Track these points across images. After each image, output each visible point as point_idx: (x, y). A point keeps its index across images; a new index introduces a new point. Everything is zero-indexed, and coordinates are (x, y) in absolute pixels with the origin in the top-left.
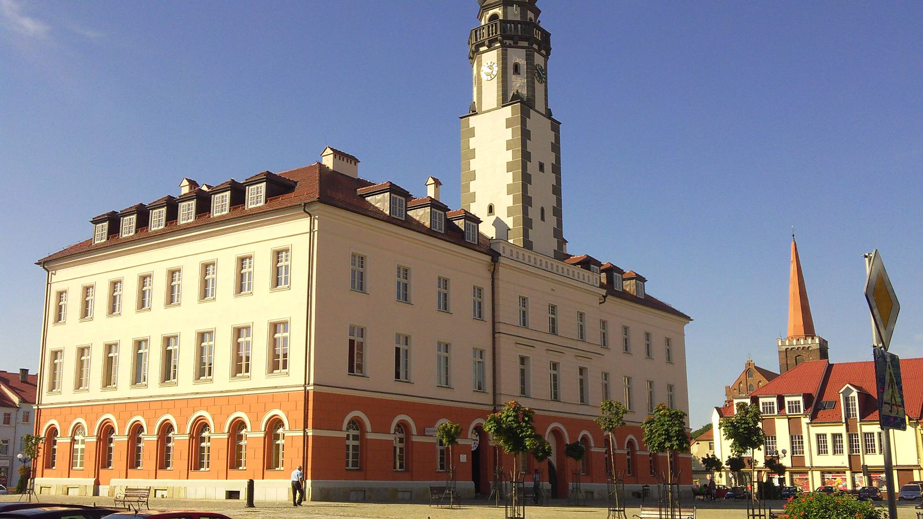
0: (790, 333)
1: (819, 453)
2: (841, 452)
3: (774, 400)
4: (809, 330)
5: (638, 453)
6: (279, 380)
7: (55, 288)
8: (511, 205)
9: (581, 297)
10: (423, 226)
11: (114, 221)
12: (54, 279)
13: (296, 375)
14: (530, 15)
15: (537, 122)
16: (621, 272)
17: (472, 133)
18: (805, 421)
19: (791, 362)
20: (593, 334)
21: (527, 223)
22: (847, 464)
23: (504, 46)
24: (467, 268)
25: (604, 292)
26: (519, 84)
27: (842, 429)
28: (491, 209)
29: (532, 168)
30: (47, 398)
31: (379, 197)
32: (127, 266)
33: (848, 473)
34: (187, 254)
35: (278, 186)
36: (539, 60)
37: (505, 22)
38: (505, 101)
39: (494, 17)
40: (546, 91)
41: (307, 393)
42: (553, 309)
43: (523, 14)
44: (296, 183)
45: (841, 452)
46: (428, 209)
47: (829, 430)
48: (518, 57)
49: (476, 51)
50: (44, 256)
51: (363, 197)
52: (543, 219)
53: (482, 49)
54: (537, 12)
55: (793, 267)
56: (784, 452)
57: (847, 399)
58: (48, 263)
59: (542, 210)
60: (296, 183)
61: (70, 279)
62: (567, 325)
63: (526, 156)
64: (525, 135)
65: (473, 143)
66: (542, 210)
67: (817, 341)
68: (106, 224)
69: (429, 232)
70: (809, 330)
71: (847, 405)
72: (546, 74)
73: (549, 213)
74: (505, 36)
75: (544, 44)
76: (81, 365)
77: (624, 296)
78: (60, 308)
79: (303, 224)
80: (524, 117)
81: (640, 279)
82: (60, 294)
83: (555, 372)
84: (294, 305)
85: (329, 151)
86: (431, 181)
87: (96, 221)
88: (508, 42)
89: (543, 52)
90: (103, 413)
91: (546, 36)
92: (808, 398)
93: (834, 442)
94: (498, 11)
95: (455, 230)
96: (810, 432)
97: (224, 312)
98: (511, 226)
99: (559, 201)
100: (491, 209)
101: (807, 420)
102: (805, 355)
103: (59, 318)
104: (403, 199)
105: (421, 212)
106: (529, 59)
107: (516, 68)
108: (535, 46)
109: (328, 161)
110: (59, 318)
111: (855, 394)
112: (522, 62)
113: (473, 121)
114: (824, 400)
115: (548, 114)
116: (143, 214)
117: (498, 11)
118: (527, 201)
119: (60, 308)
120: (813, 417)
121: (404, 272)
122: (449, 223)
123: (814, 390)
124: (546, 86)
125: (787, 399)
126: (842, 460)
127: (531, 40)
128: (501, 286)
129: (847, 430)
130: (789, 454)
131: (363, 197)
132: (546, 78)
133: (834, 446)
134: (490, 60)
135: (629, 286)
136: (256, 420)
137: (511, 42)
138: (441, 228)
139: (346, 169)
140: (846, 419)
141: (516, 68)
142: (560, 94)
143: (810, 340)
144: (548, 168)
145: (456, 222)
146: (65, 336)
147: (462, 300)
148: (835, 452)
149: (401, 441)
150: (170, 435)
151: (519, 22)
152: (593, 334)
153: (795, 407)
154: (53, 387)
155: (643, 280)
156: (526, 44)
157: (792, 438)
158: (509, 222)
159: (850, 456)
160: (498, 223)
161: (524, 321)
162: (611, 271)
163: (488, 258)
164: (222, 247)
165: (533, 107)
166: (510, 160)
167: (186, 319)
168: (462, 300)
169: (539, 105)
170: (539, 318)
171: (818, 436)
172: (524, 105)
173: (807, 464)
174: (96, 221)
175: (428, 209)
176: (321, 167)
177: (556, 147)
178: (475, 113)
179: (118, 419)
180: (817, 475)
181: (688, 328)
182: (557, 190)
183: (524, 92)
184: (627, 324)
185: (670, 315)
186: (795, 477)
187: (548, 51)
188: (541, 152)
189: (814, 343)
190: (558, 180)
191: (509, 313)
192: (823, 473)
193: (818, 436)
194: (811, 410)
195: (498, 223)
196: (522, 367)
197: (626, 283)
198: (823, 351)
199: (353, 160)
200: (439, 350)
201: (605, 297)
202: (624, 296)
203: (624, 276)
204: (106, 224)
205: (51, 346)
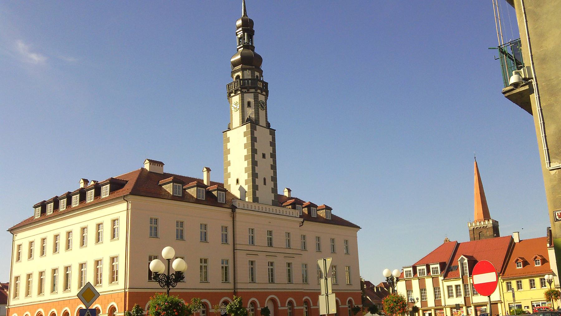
0: (476, 218)
1: (449, 297)
2: (460, 295)
3: (425, 267)
4: (486, 215)
5: (312, 307)
6: (114, 287)
7: (17, 243)
8: (247, 178)
9: (288, 223)
10: (193, 197)
11: (43, 206)
12: (16, 238)
13: (121, 285)
14: (257, 74)
15: (261, 132)
16: (316, 206)
17: (228, 140)
18: (441, 278)
19: (477, 236)
20: (296, 243)
21: (255, 188)
22: (463, 303)
23: (242, 93)
24: (216, 217)
25: (302, 220)
26: (250, 112)
27: (460, 282)
28: (237, 181)
29: (258, 157)
30: (12, 302)
31: (168, 185)
32: (48, 230)
33: (464, 308)
34: (73, 224)
35: (116, 185)
36: (261, 98)
37: (243, 80)
38: (243, 122)
39: (238, 77)
40: (266, 114)
41: (125, 293)
42: (270, 233)
43: (253, 74)
44: (127, 181)
45: (460, 295)
46: (195, 188)
47: (453, 283)
48: (250, 98)
49: (229, 96)
50: (11, 226)
51: (161, 186)
52: (265, 184)
53: (232, 95)
54: (261, 72)
55: (476, 177)
56: (417, 299)
57: (462, 264)
58: (13, 230)
59: (265, 179)
60: (127, 181)
61: (23, 237)
62: (279, 241)
63: (254, 151)
64: (253, 140)
65: (229, 146)
66: (265, 179)
67: (491, 222)
68: (40, 208)
69: (197, 201)
70: (486, 215)
71: (463, 268)
72: (266, 105)
73: (269, 181)
74: (242, 87)
75: (265, 88)
76: (28, 283)
77: (318, 220)
78: (19, 254)
79: (123, 206)
80: (253, 130)
81: (328, 208)
82: (19, 246)
83: (272, 267)
84: (119, 248)
85: (147, 161)
86: (205, 169)
87: (35, 207)
88: (244, 90)
89: (264, 93)
90: (38, 308)
91: (266, 85)
92: (443, 265)
93: (457, 290)
94: (240, 74)
95: (214, 196)
96: (444, 285)
97: (91, 253)
98: (247, 190)
99: (275, 173)
100: (237, 181)
101: (442, 278)
102: (484, 231)
103: (18, 259)
104: (181, 185)
105: (192, 190)
106: (256, 98)
107: (249, 104)
108: (259, 91)
109: (147, 167)
110: (18, 259)
111: (466, 261)
112: (252, 100)
113: (229, 134)
114: (452, 265)
115: (268, 126)
116: (56, 201)
117: (240, 74)
118: (254, 175)
119: (19, 254)
120: (445, 276)
121: (181, 224)
122: (209, 194)
123: (447, 260)
124: (266, 112)
125: (431, 267)
126: (460, 301)
127: (256, 88)
128: (238, 224)
129: (463, 283)
130: (420, 300)
131: (161, 186)
132: (266, 107)
133: (457, 292)
134: (236, 99)
135: (322, 213)
136: (104, 308)
137: (246, 90)
138: (203, 197)
139: (157, 169)
140: (462, 276)
141: (249, 104)
142: (275, 114)
143: (487, 222)
144: (268, 156)
145: (213, 192)
146: (21, 269)
147: (214, 235)
148: (457, 296)
149: (203, 312)
150: (115, 313)
151: (250, 79)
152: (296, 243)
153: (435, 271)
154: (16, 295)
155: (331, 209)
156: (253, 90)
157: (435, 289)
158: (246, 188)
159: (465, 298)
160: (241, 189)
161: (253, 241)
162: (311, 206)
163: (230, 210)
164: (90, 219)
165: (258, 124)
166: (246, 154)
167: (73, 257)
168: (214, 235)
169: (262, 122)
170: (261, 239)
171: (448, 287)
172: (252, 123)
173: (443, 304)
174: (35, 207)
175: (195, 188)
176: (143, 169)
177: (273, 144)
178: (229, 129)
179: (45, 311)
180: (448, 310)
181: (359, 233)
182: (274, 167)
183: (253, 116)
184: (318, 235)
185: (351, 228)
186: (437, 312)
187: (267, 92)
188: (263, 147)
189: (489, 224)
190: (275, 162)
191: (242, 238)
192: (451, 308)
193: (448, 287)
194: (445, 271)
195: (241, 189)
196: (252, 266)
197: (319, 213)
198: (496, 228)
199: (161, 164)
200: (201, 262)
201: (303, 222)
202: (318, 220)
203: (318, 209)
204: (40, 208)
205: (15, 274)
